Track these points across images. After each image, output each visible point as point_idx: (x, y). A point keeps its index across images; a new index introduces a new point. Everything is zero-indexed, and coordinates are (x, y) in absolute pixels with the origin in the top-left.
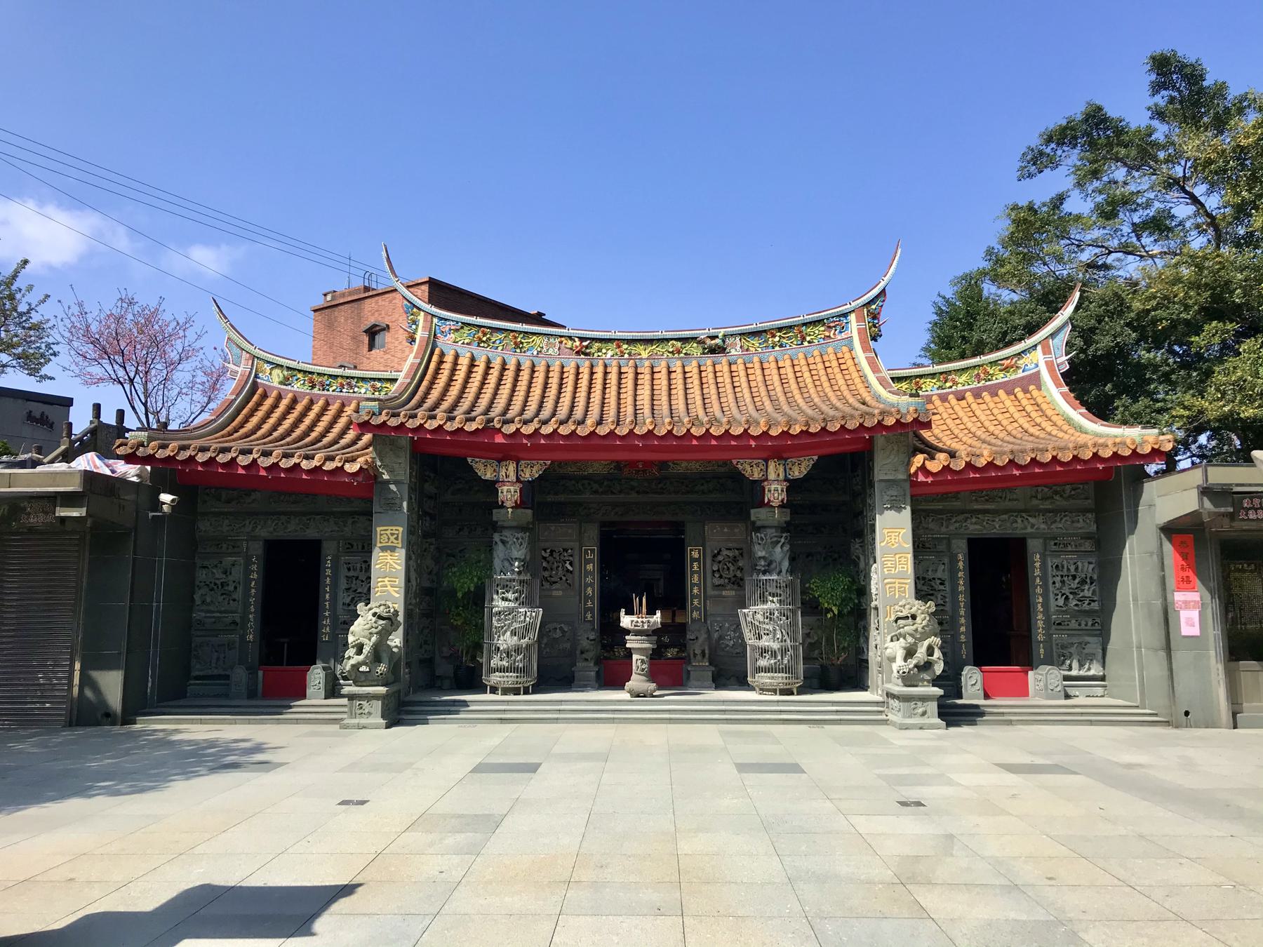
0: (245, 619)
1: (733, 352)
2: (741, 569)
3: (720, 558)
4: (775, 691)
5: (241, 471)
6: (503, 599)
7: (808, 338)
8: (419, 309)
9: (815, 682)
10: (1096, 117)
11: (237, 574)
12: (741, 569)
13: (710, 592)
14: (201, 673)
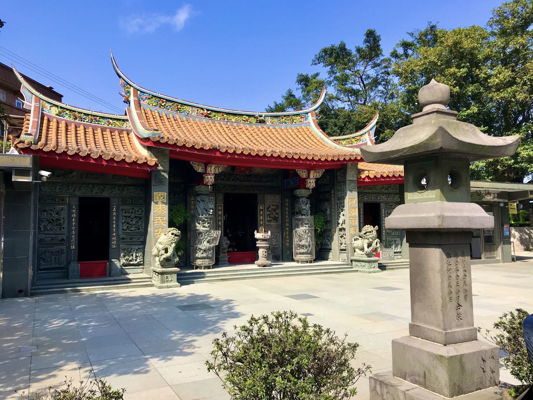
0: (69, 238)
1: (268, 124)
2: (277, 214)
3: (270, 209)
4: (307, 262)
5: (92, 161)
6: (203, 227)
7: (295, 121)
8: (130, 85)
9: (225, 256)
10: (343, 48)
11: (64, 214)
12: (277, 214)
13: (267, 223)
14: (46, 267)
